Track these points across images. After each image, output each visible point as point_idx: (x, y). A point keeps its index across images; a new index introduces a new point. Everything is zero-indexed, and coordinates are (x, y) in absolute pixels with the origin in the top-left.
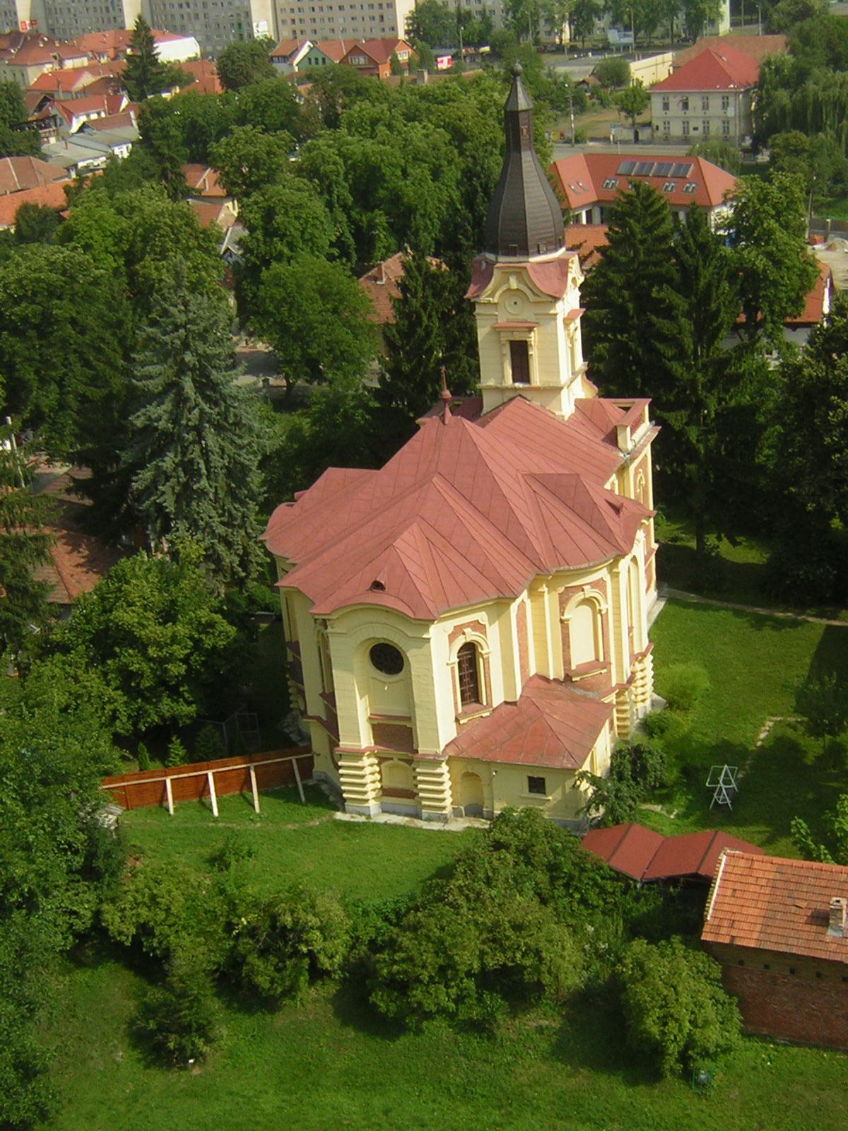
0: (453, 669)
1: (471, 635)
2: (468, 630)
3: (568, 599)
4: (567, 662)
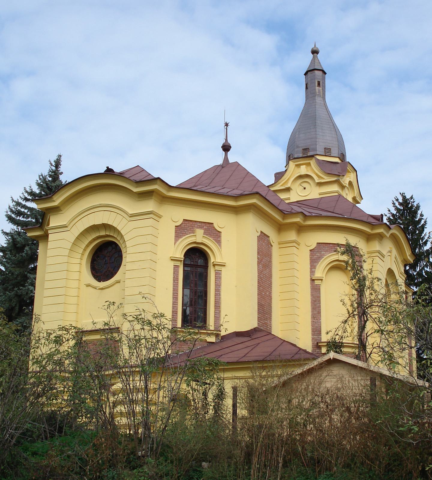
0: (176, 267)
1: (199, 237)
3: (319, 258)
4: (316, 331)
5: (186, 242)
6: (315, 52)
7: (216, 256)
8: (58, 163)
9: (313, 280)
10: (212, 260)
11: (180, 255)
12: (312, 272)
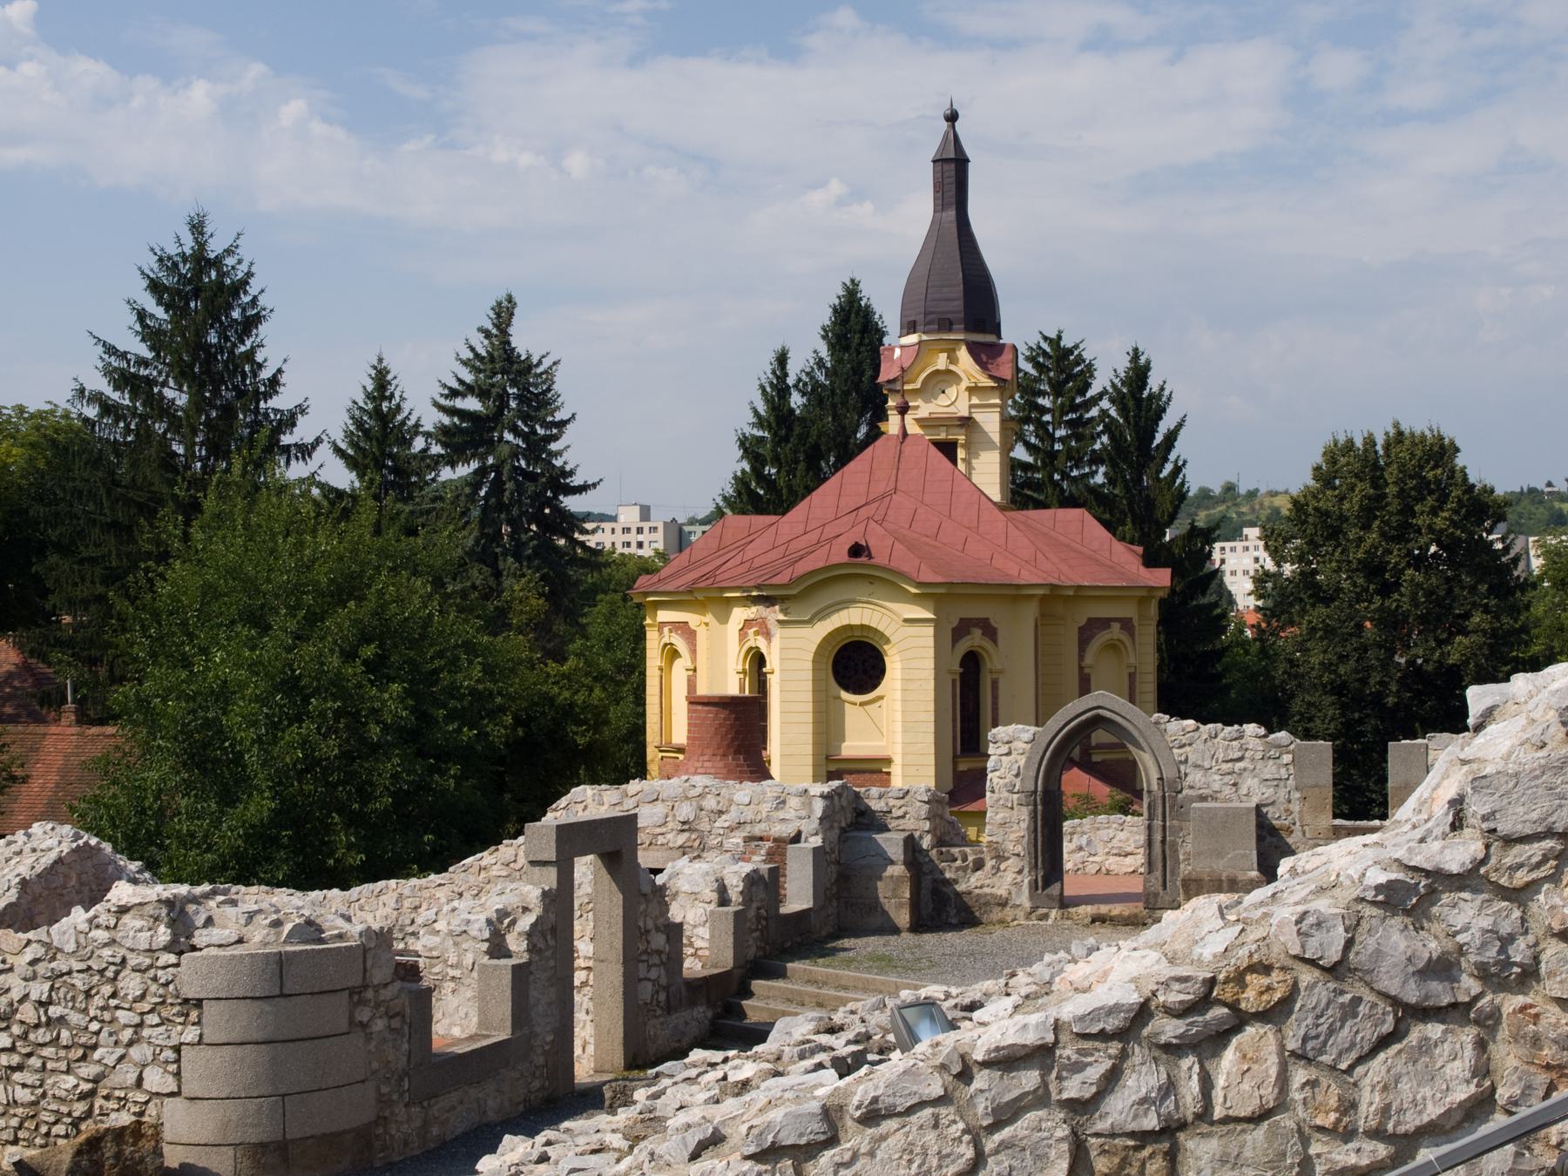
0: (954, 681)
1: (975, 639)
2: (977, 632)
5: (964, 646)
6: (952, 117)
7: (994, 660)
8: (504, 313)
9: (1081, 668)
10: (989, 665)
11: (957, 668)
12: (1081, 657)
